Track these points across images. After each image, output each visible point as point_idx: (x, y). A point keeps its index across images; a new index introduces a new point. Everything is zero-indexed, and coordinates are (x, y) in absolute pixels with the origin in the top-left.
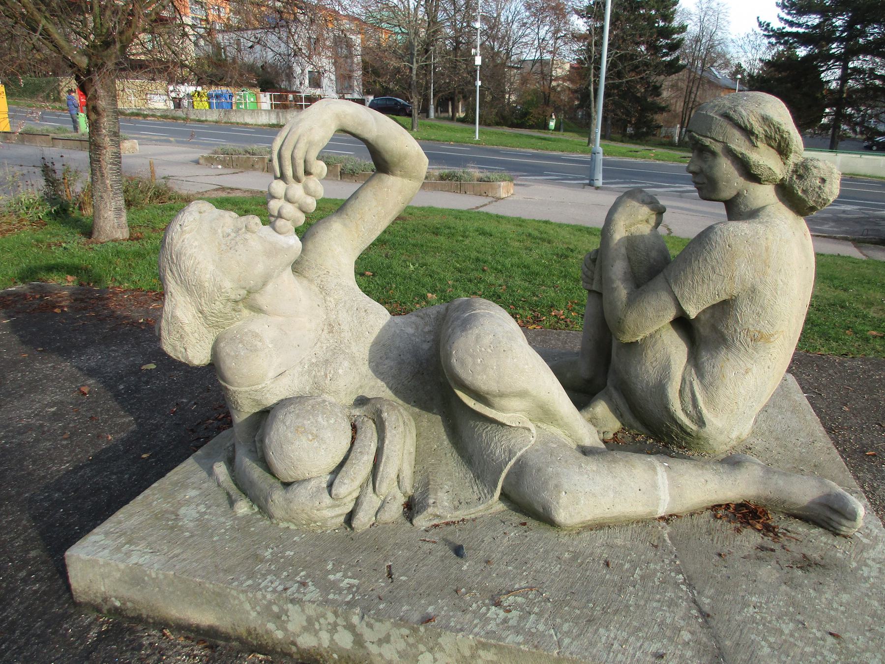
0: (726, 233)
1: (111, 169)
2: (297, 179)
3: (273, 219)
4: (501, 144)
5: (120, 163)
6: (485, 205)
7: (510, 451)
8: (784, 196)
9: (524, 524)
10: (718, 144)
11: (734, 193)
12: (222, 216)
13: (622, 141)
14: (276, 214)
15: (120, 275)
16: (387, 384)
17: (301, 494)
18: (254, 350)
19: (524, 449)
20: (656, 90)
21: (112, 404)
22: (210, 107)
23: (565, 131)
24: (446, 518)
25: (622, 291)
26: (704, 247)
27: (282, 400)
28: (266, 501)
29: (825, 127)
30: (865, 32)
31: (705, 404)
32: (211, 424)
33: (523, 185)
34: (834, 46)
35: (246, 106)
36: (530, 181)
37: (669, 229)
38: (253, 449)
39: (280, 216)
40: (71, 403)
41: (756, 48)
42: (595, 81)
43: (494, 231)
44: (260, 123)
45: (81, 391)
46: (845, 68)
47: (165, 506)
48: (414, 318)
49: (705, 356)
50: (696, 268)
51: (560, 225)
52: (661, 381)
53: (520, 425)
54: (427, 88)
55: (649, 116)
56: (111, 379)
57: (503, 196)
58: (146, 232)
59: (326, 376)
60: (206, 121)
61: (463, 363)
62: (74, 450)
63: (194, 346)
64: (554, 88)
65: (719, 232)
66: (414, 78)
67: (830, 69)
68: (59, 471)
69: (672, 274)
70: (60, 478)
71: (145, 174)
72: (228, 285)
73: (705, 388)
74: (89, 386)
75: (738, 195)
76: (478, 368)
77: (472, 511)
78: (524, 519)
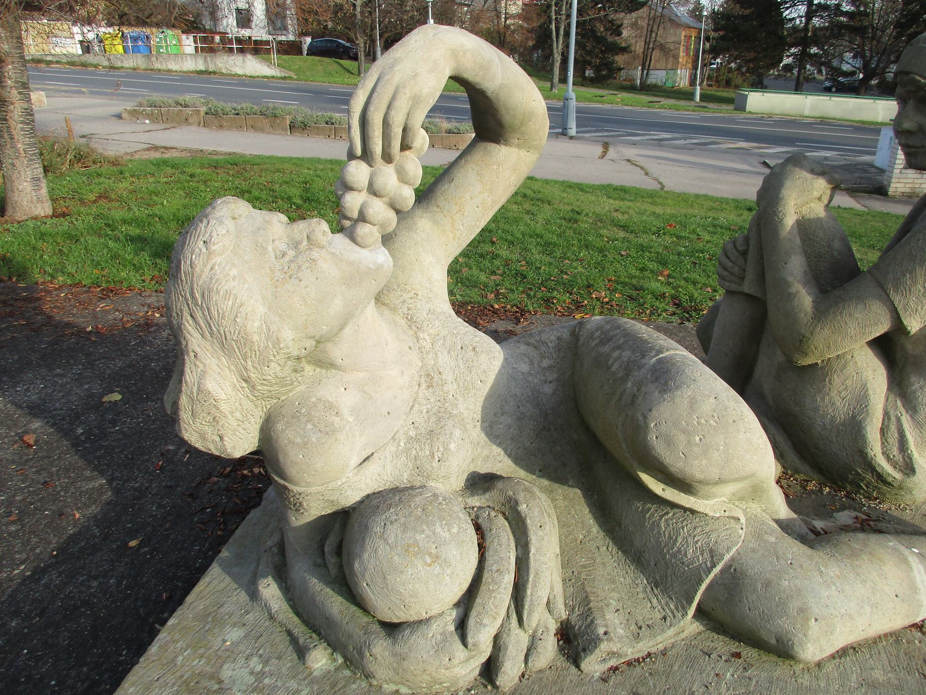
1: (22, 129)
2: (387, 158)
3: (347, 223)
5: (33, 121)
7: (711, 551)
9: (738, 655)
12: (267, 222)
13: (582, 85)
14: (355, 215)
15: (51, 265)
16: (505, 450)
17: (420, 646)
18: (330, 431)
19: (734, 549)
20: (617, 31)
21: (73, 458)
22: (125, 52)
24: (626, 655)
25: (805, 300)
27: (368, 496)
28: (361, 654)
29: (788, 68)
31: (917, 446)
32: (215, 483)
35: (167, 49)
37: (660, 183)
38: (319, 561)
39: (362, 218)
40: (13, 462)
42: (556, 19)
44: (185, 70)
45: (24, 442)
47: (199, 664)
48: (523, 348)
51: (547, 182)
52: (854, 417)
53: (727, 514)
54: (373, 29)
56: (63, 419)
58: (74, 206)
59: (433, 457)
60: (122, 67)
61: (669, 442)
62: (29, 540)
63: (234, 430)
66: (359, 16)
67: (795, 5)
68: (11, 580)
70: (15, 591)
71: (59, 130)
72: (287, 335)
74: (34, 432)
76: (696, 449)
77: (659, 638)
78: (734, 647)
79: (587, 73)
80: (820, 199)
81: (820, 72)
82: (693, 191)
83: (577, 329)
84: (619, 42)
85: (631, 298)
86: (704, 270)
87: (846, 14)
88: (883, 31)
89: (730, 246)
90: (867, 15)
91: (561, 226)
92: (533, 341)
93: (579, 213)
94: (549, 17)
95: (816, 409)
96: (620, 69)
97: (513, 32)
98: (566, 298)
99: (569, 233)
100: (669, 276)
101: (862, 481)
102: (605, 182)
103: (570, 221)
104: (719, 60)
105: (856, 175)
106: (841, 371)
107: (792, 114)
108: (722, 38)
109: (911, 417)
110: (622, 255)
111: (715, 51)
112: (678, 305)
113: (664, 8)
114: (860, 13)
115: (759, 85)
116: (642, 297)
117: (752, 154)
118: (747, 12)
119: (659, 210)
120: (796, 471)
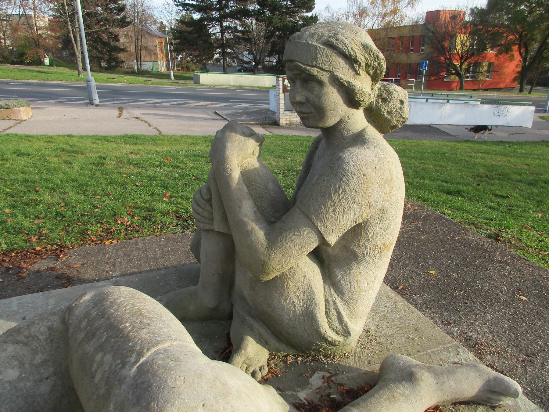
0: (358, 163)
4: (8, 77)
6: (11, 127)
8: (370, 118)
10: (324, 73)
11: (338, 120)
13: (101, 72)
20: (116, 38)
23: (57, 66)
25: (259, 234)
26: (342, 179)
29: (217, 60)
30: (228, 6)
31: (348, 317)
33: (39, 108)
34: (214, 13)
36: (43, 104)
37: (159, 130)
41: (170, 12)
43: (30, 151)
46: (222, 26)
49: (339, 274)
50: (337, 200)
51: (82, 137)
55: (115, 55)
57: (24, 118)
64: (40, 35)
65: (351, 162)
67: (214, 26)
69: (312, 209)
73: (347, 303)
75: (341, 121)
79: (102, 64)
80: (253, 154)
81: (234, 62)
82: (179, 133)
83: (67, 316)
84: (119, 45)
85: (147, 219)
86: (192, 189)
87: (240, 31)
88: (259, 41)
89: (198, 196)
90: (250, 32)
91: (92, 169)
92: (22, 338)
93: (104, 158)
94: (69, 31)
95: (283, 309)
96: (123, 62)
97: (45, 39)
98: (98, 228)
99: (98, 174)
100: (170, 197)
101: (320, 348)
102: (122, 133)
103: (98, 164)
104: (180, 56)
105: (263, 116)
106: (293, 277)
107: (225, 84)
108: (179, 43)
109: (342, 299)
110: (137, 186)
111: (177, 51)
112: (179, 217)
113: (142, 26)
114: (247, 31)
115: (205, 69)
116: (154, 217)
117: (209, 108)
118: (190, 29)
119: (159, 149)
120: (278, 351)
